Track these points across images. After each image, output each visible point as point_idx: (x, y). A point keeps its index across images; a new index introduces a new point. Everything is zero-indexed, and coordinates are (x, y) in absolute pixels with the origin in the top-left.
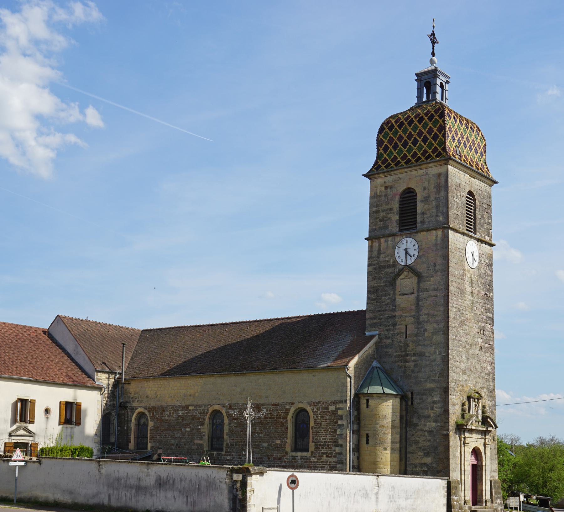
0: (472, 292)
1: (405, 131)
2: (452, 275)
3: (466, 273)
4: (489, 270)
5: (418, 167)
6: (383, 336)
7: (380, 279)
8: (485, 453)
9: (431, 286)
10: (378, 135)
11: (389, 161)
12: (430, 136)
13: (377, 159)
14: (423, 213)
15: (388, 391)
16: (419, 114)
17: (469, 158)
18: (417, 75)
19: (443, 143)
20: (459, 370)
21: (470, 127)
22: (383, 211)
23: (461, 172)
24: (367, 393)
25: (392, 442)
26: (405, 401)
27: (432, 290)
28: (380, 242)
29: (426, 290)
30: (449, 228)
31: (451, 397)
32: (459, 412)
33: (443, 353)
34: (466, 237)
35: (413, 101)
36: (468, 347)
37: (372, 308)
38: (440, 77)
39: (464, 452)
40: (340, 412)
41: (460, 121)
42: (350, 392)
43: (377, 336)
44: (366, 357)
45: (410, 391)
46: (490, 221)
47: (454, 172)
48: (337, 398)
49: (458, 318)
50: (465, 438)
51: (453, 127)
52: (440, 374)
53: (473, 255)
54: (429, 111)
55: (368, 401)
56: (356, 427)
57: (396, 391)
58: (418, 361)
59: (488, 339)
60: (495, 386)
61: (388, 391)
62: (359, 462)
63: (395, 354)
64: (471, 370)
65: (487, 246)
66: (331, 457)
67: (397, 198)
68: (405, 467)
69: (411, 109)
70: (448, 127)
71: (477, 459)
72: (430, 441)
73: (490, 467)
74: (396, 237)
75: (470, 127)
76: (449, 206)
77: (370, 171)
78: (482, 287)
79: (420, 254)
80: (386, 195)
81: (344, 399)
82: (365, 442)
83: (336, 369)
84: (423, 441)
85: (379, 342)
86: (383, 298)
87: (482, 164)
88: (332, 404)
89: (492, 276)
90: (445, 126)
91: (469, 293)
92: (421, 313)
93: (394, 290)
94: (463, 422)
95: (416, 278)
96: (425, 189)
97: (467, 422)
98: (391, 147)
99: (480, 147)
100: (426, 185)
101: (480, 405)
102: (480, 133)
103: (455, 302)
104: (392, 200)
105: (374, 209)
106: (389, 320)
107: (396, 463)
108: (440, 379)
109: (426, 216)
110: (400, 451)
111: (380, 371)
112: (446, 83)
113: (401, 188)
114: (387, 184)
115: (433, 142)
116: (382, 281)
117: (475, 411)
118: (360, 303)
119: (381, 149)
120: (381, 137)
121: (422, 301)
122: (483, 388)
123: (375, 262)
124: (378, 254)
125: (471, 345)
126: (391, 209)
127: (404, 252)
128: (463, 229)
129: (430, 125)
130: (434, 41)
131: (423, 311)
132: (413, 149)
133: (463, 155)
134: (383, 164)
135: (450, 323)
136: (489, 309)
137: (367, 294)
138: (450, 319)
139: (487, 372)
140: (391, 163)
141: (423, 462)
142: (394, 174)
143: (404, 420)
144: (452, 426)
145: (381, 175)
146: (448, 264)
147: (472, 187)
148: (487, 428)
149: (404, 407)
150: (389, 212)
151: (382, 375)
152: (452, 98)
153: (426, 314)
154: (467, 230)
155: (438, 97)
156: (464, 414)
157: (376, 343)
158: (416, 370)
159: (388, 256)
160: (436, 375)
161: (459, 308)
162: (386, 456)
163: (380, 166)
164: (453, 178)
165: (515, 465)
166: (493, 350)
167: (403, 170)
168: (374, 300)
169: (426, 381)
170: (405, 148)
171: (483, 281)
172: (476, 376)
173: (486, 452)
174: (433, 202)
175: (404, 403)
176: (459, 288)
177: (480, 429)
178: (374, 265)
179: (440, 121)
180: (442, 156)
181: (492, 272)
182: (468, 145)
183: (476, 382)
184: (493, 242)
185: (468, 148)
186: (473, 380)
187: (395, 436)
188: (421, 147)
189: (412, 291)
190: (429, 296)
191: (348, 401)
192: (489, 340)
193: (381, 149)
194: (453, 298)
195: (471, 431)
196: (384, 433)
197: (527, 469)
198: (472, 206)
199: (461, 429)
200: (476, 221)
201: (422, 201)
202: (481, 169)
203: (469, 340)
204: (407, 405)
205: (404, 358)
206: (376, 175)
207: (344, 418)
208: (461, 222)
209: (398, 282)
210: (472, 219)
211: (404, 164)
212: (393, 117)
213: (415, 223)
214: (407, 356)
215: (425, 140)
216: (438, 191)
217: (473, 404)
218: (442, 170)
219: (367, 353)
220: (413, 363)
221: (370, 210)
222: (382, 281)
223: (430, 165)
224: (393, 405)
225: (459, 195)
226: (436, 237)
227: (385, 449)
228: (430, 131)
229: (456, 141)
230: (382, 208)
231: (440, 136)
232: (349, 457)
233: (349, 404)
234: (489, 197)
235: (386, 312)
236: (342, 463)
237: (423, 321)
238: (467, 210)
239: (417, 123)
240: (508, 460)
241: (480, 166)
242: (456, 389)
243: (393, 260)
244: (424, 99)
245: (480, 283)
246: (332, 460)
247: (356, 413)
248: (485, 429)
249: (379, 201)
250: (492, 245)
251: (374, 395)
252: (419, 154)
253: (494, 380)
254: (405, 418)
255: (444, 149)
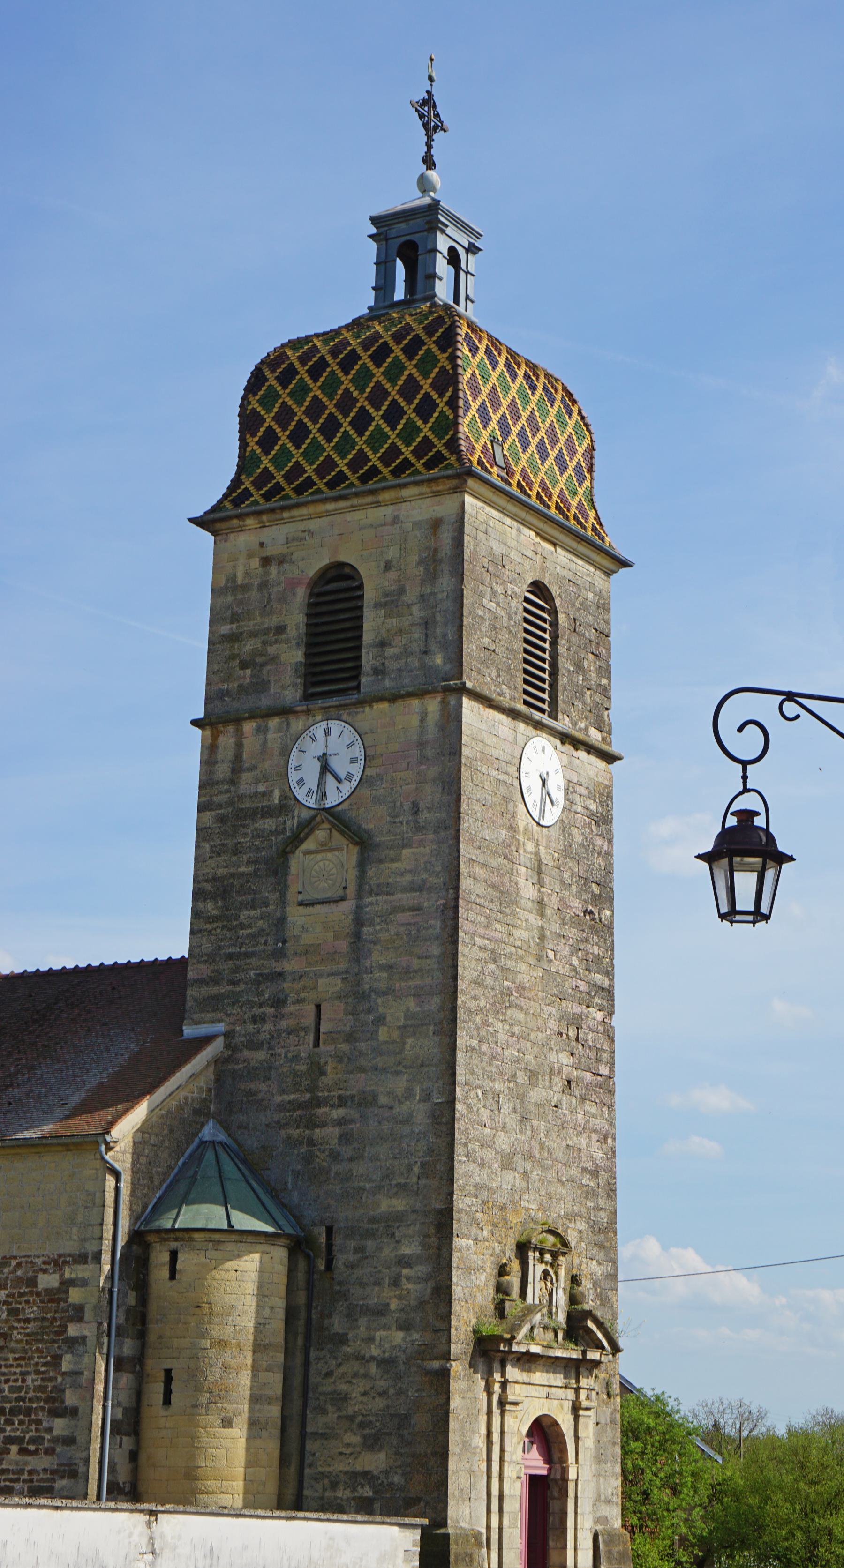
0: (540, 903)
1: (330, 387)
2: (471, 841)
3: (521, 838)
4: (601, 835)
5: (369, 499)
6: (238, 1040)
7: (237, 850)
8: (577, 1438)
9: (402, 875)
10: (244, 398)
11: (279, 478)
12: (410, 402)
13: (238, 473)
14: (382, 644)
15: (244, 1221)
16: (376, 336)
17: (536, 481)
18: (375, 220)
19: (448, 427)
20: (489, 1155)
21: (540, 386)
22: (254, 634)
23: (508, 521)
24: (173, 1230)
25: (255, 1399)
26: (308, 1257)
27: (405, 890)
28: (239, 734)
29: (386, 889)
30: (462, 690)
31: (458, 1242)
32: (486, 1297)
33: (435, 1094)
34: (522, 726)
35: (363, 300)
36: (522, 1078)
37: (207, 946)
38: (449, 231)
39: (502, 1432)
40: (75, 1295)
41: (508, 365)
42: (115, 1224)
43: (221, 1039)
44: (180, 1108)
45: (322, 1222)
46: (604, 681)
47: (482, 517)
48: (70, 1246)
49: (489, 981)
50: (504, 1385)
51: (486, 379)
52: (423, 1165)
53: (544, 783)
54: (408, 329)
55: (174, 1255)
56: (128, 1348)
57: (275, 1223)
58: (352, 1121)
59: (593, 1055)
60: (614, 1213)
61: (244, 1221)
62: (135, 1471)
63: (278, 1099)
64: (531, 1156)
65: (593, 759)
66: (36, 1452)
67: (301, 594)
68: (296, 1487)
69: (357, 324)
70: (465, 377)
71: (548, 1458)
72: (383, 1394)
73: (591, 1486)
74: (292, 719)
75: (540, 386)
76: (466, 621)
77: (214, 509)
78: (574, 889)
79: (369, 772)
80: (264, 585)
81: (91, 1248)
82: (160, 1398)
83: (67, 1147)
84: (363, 1395)
85: (226, 1061)
86: (244, 915)
87: (580, 503)
88: (50, 1267)
89: (609, 854)
90: (456, 375)
91: (530, 905)
92: (368, 963)
93: (282, 888)
94: (498, 1330)
95: (355, 850)
96: (388, 566)
97: (514, 1329)
98: (284, 437)
99: (573, 452)
100: (392, 554)
101: (562, 1273)
102: (575, 409)
103: (481, 931)
104: (282, 599)
105: (225, 629)
106: (263, 986)
107: (269, 1474)
108: (423, 1182)
109: (390, 651)
110: (283, 1429)
111: (224, 1157)
112: (467, 251)
113: (314, 564)
114: (269, 552)
115: (419, 423)
116: (245, 858)
117: (545, 1294)
118: (162, 933)
119: (252, 442)
120: (254, 404)
121: (372, 924)
122: (572, 1217)
123: (223, 798)
124: (233, 771)
125: (533, 1075)
126: (281, 629)
127: (318, 765)
128: (513, 699)
129: (411, 369)
130: (432, 125)
131: (375, 955)
132: (355, 443)
133: (518, 470)
134: (259, 488)
135: (461, 999)
136: (598, 959)
137: (195, 900)
138: (461, 985)
139: (590, 1166)
140: (284, 484)
141: (359, 1468)
142: (292, 519)
143: (301, 1322)
144: (460, 1343)
145: (250, 522)
146: (458, 806)
147: (544, 569)
148: (584, 1353)
149: (301, 1276)
150: (271, 637)
151: (229, 1168)
152: (485, 296)
153: (382, 968)
154: (526, 703)
155: (443, 291)
156: (502, 1302)
157: (217, 1061)
158: (347, 1151)
159: (266, 778)
160: (409, 1168)
161: (493, 951)
162: (230, 1448)
163: (247, 494)
164: (481, 536)
165: (718, 1492)
166: (611, 1092)
167: (321, 508)
168: (215, 919)
169: (379, 1188)
170: (329, 441)
171: (579, 870)
172: (551, 1175)
173: (581, 1434)
174: (415, 610)
175: (302, 1264)
176: (494, 886)
177: (559, 1353)
178: (220, 806)
179: (442, 357)
180: (445, 464)
181: (610, 842)
182: (534, 442)
183: (550, 1196)
184: (615, 749)
185: (532, 448)
186: (537, 1191)
187: (263, 1376)
188: (378, 438)
189: (340, 892)
190: (395, 910)
191: (106, 1257)
192: (598, 1060)
193: (252, 442)
194: (472, 916)
195: (528, 1360)
196: (226, 1368)
197: (753, 1501)
198: (544, 630)
199: (490, 1352)
200: (552, 677)
201: (377, 605)
202: (576, 518)
203: (529, 1057)
204: (311, 1270)
205: (307, 1113)
206: (235, 522)
207: (88, 1315)
208: (504, 676)
209: (296, 862)
210: (543, 670)
211: (356, 482)
212: (294, 344)
213: (355, 673)
214: (318, 1106)
215: (393, 415)
216: (432, 576)
217: (536, 1269)
218: (444, 507)
219: (182, 1094)
220: (337, 1131)
221: (211, 632)
222: (245, 858)
223: (406, 492)
224: (261, 1271)
225: (499, 589)
226: (422, 720)
227: (228, 1423)
228: (410, 389)
229: (493, 425)
230: (249, 625)
231: (442, 404)
232: (99, 1451)
233: (107, 1268)
234: (604, 607)
235: (254, 961)
236: (73, 1474)
237: (372, 990)
238: (526, 641)
239: (370, 365)
240: (694, 1474)
241: (573, 510)
242: (479, 1216)
243: (282, 791)
244: (399, 294)
245: (567, 876)
246: (41, 1462)
247: (131, 1299)
248: (575, 1355)
249: (241, 603)
250: (610, 758)
251: (196, 1235)
252: (374, 459)
253: (611, 1191)
254: (303, 1315)
255: (453, 445)
